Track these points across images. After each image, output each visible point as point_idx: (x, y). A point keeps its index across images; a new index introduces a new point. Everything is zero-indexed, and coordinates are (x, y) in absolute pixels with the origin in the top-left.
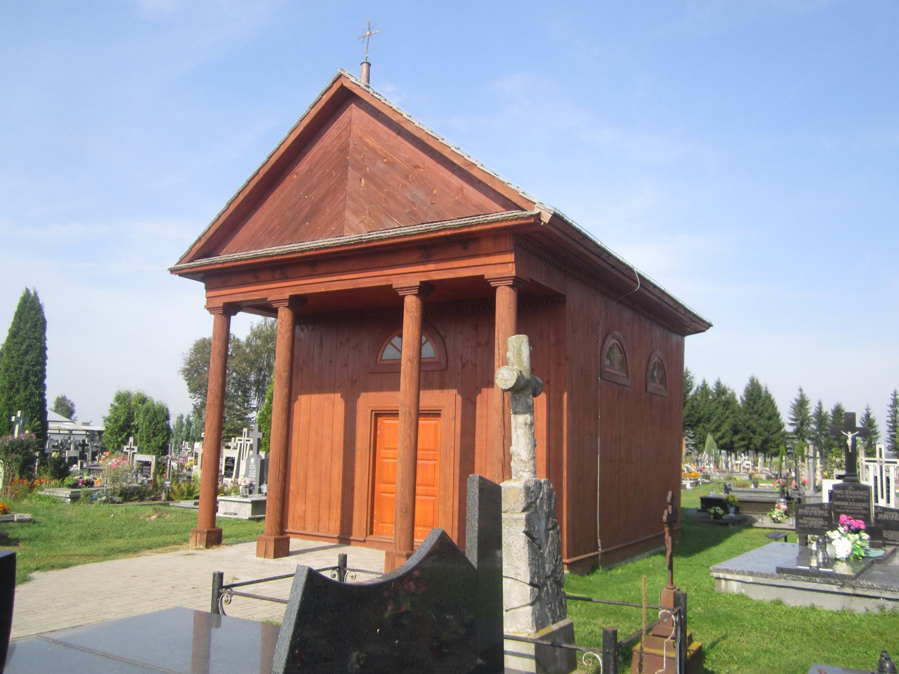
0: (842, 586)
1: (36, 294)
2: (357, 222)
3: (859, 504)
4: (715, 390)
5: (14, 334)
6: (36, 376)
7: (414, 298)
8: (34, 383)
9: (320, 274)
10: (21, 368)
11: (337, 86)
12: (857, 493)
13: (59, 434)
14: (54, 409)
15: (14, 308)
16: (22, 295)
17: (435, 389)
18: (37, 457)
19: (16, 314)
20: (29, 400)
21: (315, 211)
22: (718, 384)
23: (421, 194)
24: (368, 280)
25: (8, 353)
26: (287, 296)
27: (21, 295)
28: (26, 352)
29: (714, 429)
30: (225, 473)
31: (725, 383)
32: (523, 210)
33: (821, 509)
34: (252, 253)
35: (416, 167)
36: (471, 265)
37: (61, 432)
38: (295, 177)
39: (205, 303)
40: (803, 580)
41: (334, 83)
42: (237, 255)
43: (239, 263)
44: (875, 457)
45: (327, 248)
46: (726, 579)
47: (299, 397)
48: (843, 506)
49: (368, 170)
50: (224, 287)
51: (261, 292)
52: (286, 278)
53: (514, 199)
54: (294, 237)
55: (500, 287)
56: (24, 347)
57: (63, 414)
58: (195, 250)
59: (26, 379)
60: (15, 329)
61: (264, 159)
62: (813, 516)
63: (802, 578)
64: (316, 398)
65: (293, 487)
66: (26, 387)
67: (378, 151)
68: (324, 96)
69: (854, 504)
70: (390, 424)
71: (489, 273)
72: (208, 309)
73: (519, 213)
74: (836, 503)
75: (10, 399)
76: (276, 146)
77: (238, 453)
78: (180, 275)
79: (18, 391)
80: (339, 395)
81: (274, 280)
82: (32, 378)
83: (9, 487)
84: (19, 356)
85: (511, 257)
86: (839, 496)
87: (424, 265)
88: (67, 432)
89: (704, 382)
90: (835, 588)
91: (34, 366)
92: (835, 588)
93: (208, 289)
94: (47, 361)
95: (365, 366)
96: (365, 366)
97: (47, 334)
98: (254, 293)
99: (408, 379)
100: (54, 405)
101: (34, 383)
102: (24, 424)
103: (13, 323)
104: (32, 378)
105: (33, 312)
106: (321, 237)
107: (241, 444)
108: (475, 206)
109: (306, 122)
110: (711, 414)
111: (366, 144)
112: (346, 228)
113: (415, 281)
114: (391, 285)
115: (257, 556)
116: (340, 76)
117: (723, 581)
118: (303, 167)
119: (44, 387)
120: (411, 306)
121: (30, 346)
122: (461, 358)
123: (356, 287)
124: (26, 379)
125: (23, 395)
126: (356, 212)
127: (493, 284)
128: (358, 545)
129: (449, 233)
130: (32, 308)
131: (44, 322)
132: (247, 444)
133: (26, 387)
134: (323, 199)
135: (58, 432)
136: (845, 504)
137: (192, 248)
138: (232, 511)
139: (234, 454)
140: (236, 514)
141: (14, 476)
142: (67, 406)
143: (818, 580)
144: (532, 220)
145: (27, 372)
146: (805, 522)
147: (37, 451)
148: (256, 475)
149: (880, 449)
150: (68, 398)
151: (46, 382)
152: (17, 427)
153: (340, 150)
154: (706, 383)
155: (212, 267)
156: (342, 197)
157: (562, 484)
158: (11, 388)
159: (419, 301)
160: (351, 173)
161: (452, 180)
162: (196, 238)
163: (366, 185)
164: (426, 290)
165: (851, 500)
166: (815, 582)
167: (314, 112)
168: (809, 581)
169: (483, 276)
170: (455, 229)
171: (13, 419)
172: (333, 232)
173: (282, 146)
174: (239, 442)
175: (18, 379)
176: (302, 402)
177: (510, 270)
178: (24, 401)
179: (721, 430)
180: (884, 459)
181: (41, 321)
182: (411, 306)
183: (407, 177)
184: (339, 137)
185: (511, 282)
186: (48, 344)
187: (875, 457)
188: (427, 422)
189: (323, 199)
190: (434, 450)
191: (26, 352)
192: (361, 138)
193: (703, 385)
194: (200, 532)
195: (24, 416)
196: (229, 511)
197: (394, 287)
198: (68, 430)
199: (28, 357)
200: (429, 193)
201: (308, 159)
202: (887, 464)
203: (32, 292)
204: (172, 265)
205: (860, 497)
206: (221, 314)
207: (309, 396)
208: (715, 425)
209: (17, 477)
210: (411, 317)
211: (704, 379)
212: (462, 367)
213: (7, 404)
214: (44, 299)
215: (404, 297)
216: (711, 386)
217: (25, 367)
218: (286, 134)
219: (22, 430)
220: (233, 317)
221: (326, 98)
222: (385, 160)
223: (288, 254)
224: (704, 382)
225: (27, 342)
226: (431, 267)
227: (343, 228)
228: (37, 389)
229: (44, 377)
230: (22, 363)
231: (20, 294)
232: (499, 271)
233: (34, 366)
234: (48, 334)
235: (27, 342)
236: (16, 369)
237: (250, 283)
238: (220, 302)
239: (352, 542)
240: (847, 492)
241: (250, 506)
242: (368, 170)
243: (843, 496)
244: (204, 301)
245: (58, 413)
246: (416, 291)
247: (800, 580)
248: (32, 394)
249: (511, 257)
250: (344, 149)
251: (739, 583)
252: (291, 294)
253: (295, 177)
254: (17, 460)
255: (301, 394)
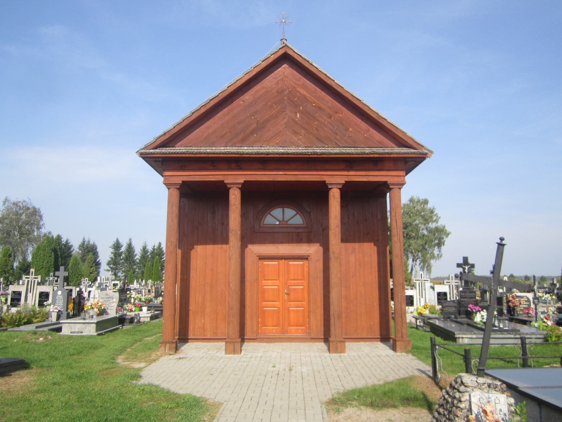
0: (515, 335)
2: (296, 139)
9: (269, 169)
12: (471, 294)
17: (304, 243)
21: (261, 127)
24: (306, 176)
26: (242, 181)
30: (11, 304)
32: (416, 149)
33: (454, 303)
34: (281, 150)
36: (379, 175)
40: (499, 334)
42: (194, 150)
46: (462, 338)
47: (195, 247)
48: (465, 301)
49: (301, 108)
50: (183, 170)
51: (217, 176)
52: (241, 169)
53: (410, 142)
54: (243, 141)
55: (333, 189)
62: (450, 306)
63: (498, 333)
64: (210, 248)
65: (192, 307)
67: (308, 98)
68: (272, 56)
69: (470, 299)
71: (328, 180)
72: (164, 184)
73: (413, 151)
74: (462, 299)
77: (26, 288)
86: (463, 296)
87: (348, 171)
90: (512, 336)
92: (512, 336)
95: (251, 228)
96: (251, 228)
98: (210, 176)
99: (337, 238)
107: (28, 281)
108: (378, 142)
111: (299, 92)
115: (226, 354)
117: (461, 339)
122: (322, 225)
123: (298, 180)
127: (228, 186)
128: (250, 342)
129: (376, 156)
132: (34, 281)
134: (268, 121)
136: (466, 300)
137: (157, 139)
138: (77, 330)
139: (22, 289)
140: (82, 332)
143: (505, 333)
146: (447, 309)
148: (63, 303)
153: (278, 92)
155: (167, 155)
157: (388, 296)
161: (361, 125)
162: (161, 133)
163: (300, 117)
165: (468, 298)
166: (504, 334)
168: (502, 334)
172: (277, 144)
173: (238, 81)
174: (27, 280)
176: (199, 251)
185: (178, 187)
189: (268, 121)
190: (302, 280)
194: (169, 342)
196: (73, 331)
197: (225, 182)
201: (252, 93)
202: (424, 281)
205: (472, 296)
206: (239, 188)
207: (204, 246)
210: (337, 201)
212: (323, 231)
222: (314, 105)
232: (396, 180)
237: (208, 169)
239: (245, 340)
240: (466, 294)
241: (94, 325)
242: (301, 108)
243: (465, 296)
246: (240, 186)
247: (497, 334)
251: (469, 339)
252: (347, 180)
255: (197, 245)
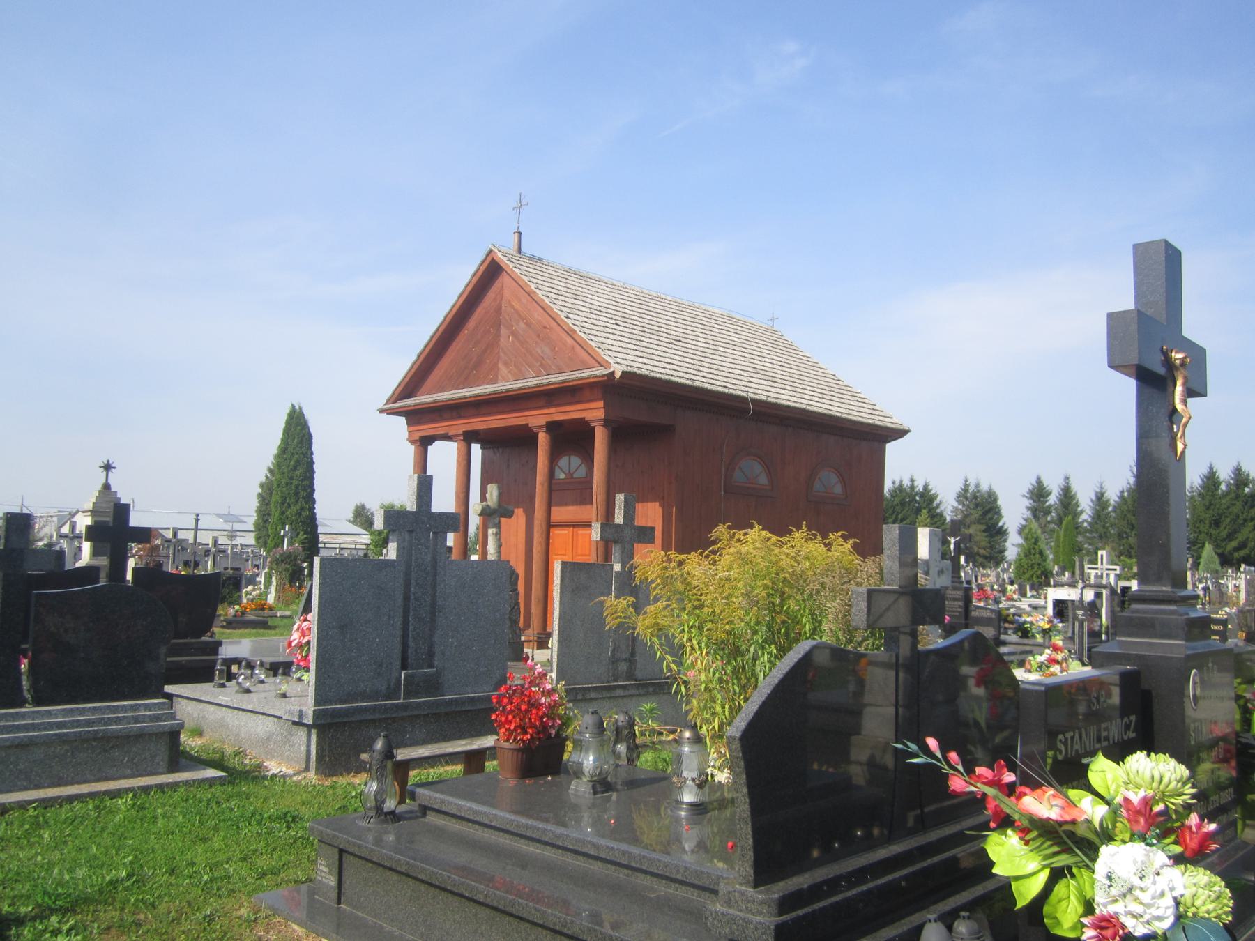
1: (300, 409)
3: (956, 603)
4: (1232, 479)
5: (284, 450)
6: (305, 490)
7: (544, 434)
8: (303, 498)
10: (291, 483)
11: (489, 259)
13: (355, 549)
14: (352, 519)
15: (285, 417)
16: (288, 411)
18: (305, 568)
19: (284, 431)
20: (300, 514)
21: (478, 364)
22: (1238, 471)
23: (547, 350)
25: (279, 469)
27: (288, 411)
28: (295, 468)
29: (1225, 536)
31: (935, 488)
35: (545, 327)
37: (358, 547)
38: (466, 332)
39: (407, 437)
41: (487, 256)
43: (425, 406)
44: (1097, 564)
45: (480, 396)
52: (460, 417)
54: (466, 384)
56: (292, 463)
57: (361, 526)
58: (396, 394)
59: (296, 494)
60: (283, 446)
61: (442, 318)
66: (296, 502)
70: (559, 534)
75: (283, 513)
76: (442, 318)
78: (388, 414)
79: (289, 506)
80: (522, 509)
81: (452, 419)
82: (302, 493)
83: (281, 595)
84: (289, 472)
85: (601, 404)
88: (364, 547)
89: (1211, 468)
91: (302, 480)
93: (409, 424)
94: (315, 476)
97: (314, 448)
100: (352, 515)
101: (303, 498)
102: (292, 538)
103: (282, 440)
104: (302, 493)
105: (299, 428)
106: (483, 384)
109: (469, 288)
110: (1220, 515)
111: (512, 307)
112: (500, 377)
113: (542, 421)
114: (528, 425)
116: (491, 251)
118: (471, 323)
119: (314, 501)
120: (543, 438)
121: (298, 461)
124: (296, 494)
125: (294, 509)
126: (506, 364)
129: (556, 386)
130: (297, 425)
131: (310, 437)
133: (296, 502)
135: (353, 546)
141: (284, 584)
142: (367, 516)
144: (606, 378)
145: (297, 487)
147: (305, 562)
149: (1102, 556)
150: (367, 506)
151: (315, 496)
152: (286, 540)
154: (930, 487)
156: (497, 352)
158: (283, 503)
159: (548, 437)
160: (503, 331)
162: (396, 384)
164: (552, 427)
167: (475, 280)
169: (584, 418)
170: (559, 383)
171: (282, 533)
175: (289, 494)
177: (601, 414)
178: (296, 515)
179: (1237, 538)
180: (1105, 566)
181: (307, 436)
182: (543, 438)
183: (539, 336)
184: (495, 299)
186: (315, 458)
187: (1097, 564)
188: (584, 532)
190: (589, 555)
191: (295, 468)
192: (509, 301)
193: (1209, 473)
195: (292, 529)
198: (366, 544)
199: (298, 472)
200: (553, 350)
202: (1107, 572)
203: (297, 407)
204: (381, 405)
208: (1226, 531)
209: (287, 586)
211: (1211, 465)
213: (281, 519)
214: (309, 414)
215: (538, 433)
216: (1225, 474)
217: (295, 482)
218: (456, 298)
219: (291, 543)
220: (429, 447)
221: (482, 269)
223: (456, 399)
224: (1211, 468)
225: (295, 457)
226: (553, 410)
227: (497, 376)
228: (306, 503)
229: (313, 491)
230: (291, 478)
231: (286, 411)
232: (595, 414)
233: (302, 480)
234: (315, 448)
235: (295, 457)
236: (287, 484)
238: (417, 436)
244: (406, 435)
245: (356, 525)
248: (302, 509)
249: (601, 404)
250: (498, 310)
253: (466, 332)
254: (286, 570)
